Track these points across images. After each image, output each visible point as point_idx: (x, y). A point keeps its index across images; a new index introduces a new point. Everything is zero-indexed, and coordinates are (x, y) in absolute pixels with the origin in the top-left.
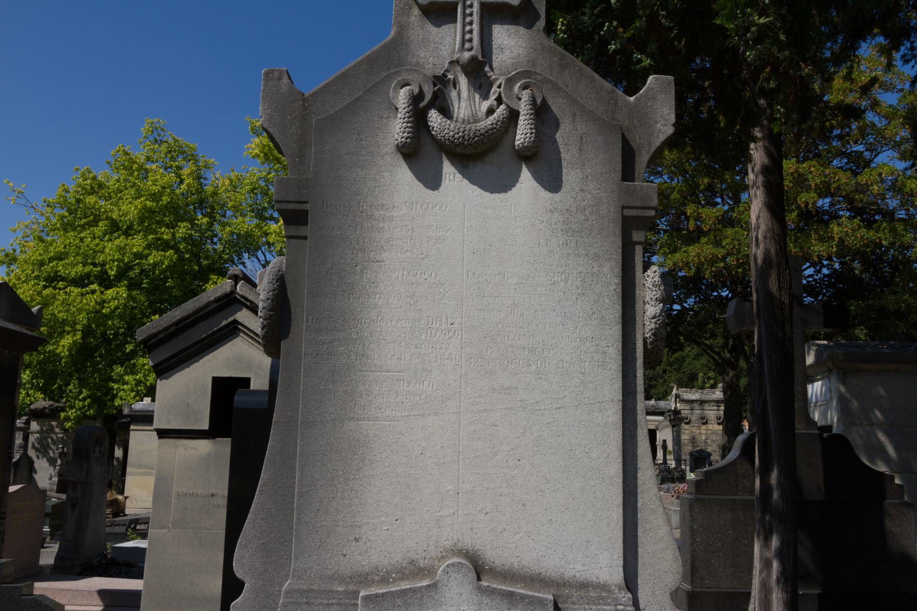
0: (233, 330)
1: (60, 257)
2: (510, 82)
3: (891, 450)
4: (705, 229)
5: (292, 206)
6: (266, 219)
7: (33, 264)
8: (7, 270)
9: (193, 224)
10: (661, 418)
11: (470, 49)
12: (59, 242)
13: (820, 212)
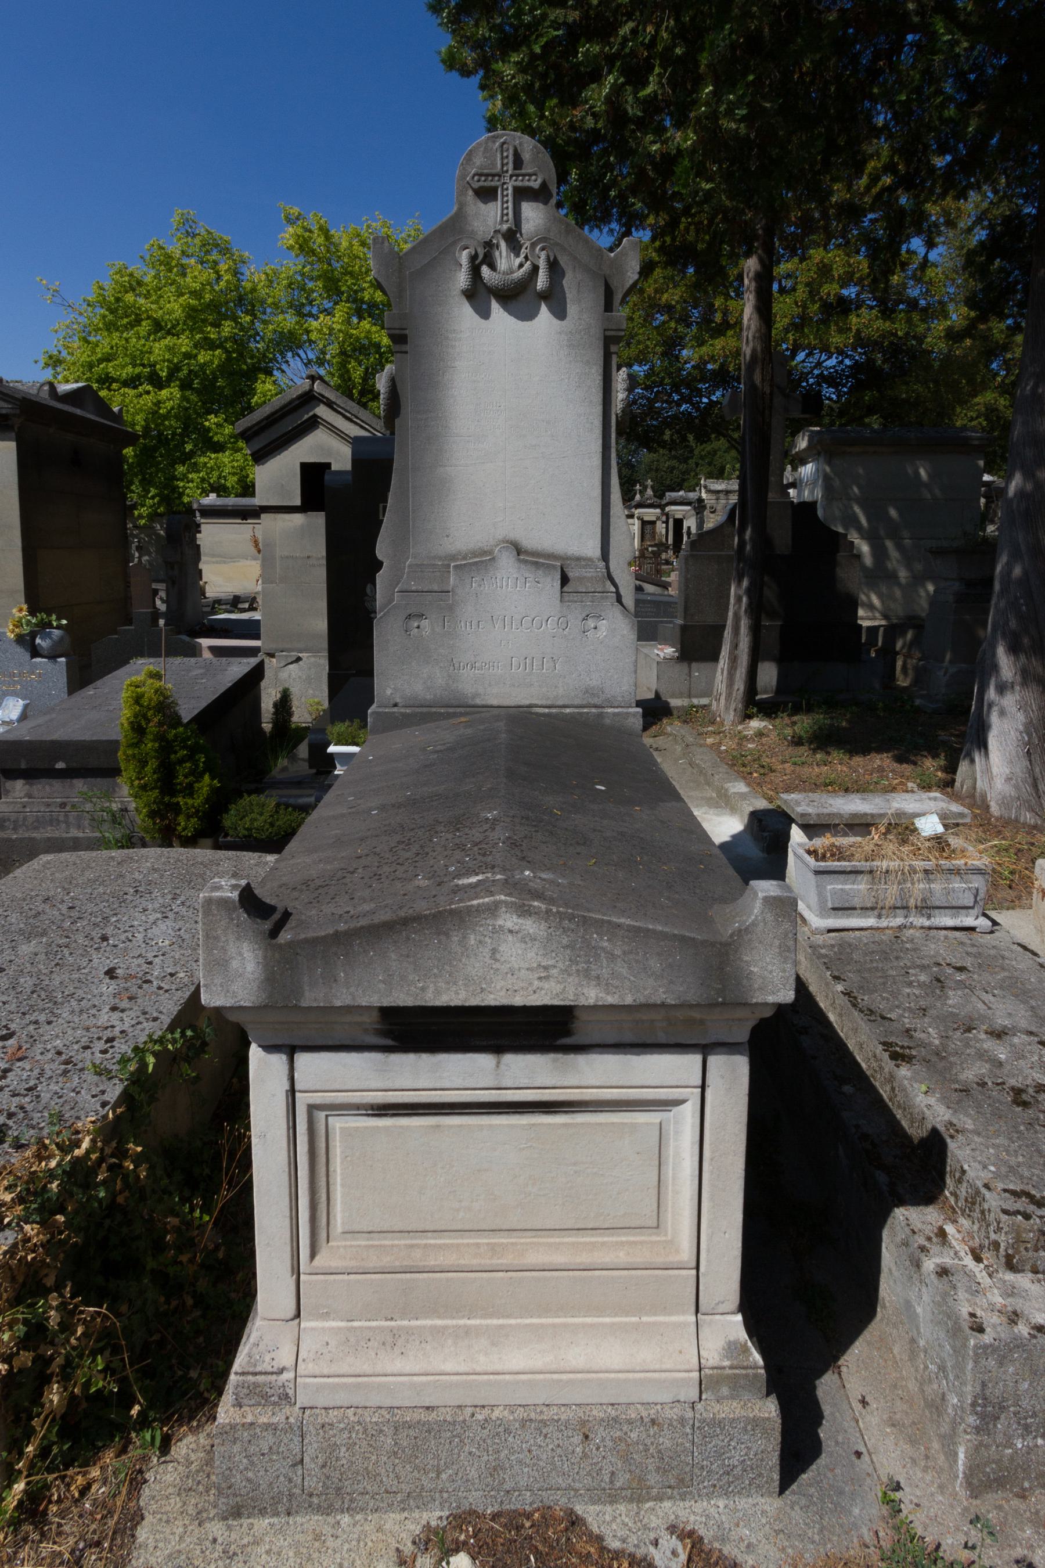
0: (314, 423)
1: (107, 359)
2: (533, 245)
3: (864, 521)
4: (732, 322)
5: (397, 332)
6: (306, 315)
7: (82, 366)
8: (53, 372)
9: (237, 323)
10: (689, 508)
11: (507, 221)
12: (105, 343)
13: (842, 300)
